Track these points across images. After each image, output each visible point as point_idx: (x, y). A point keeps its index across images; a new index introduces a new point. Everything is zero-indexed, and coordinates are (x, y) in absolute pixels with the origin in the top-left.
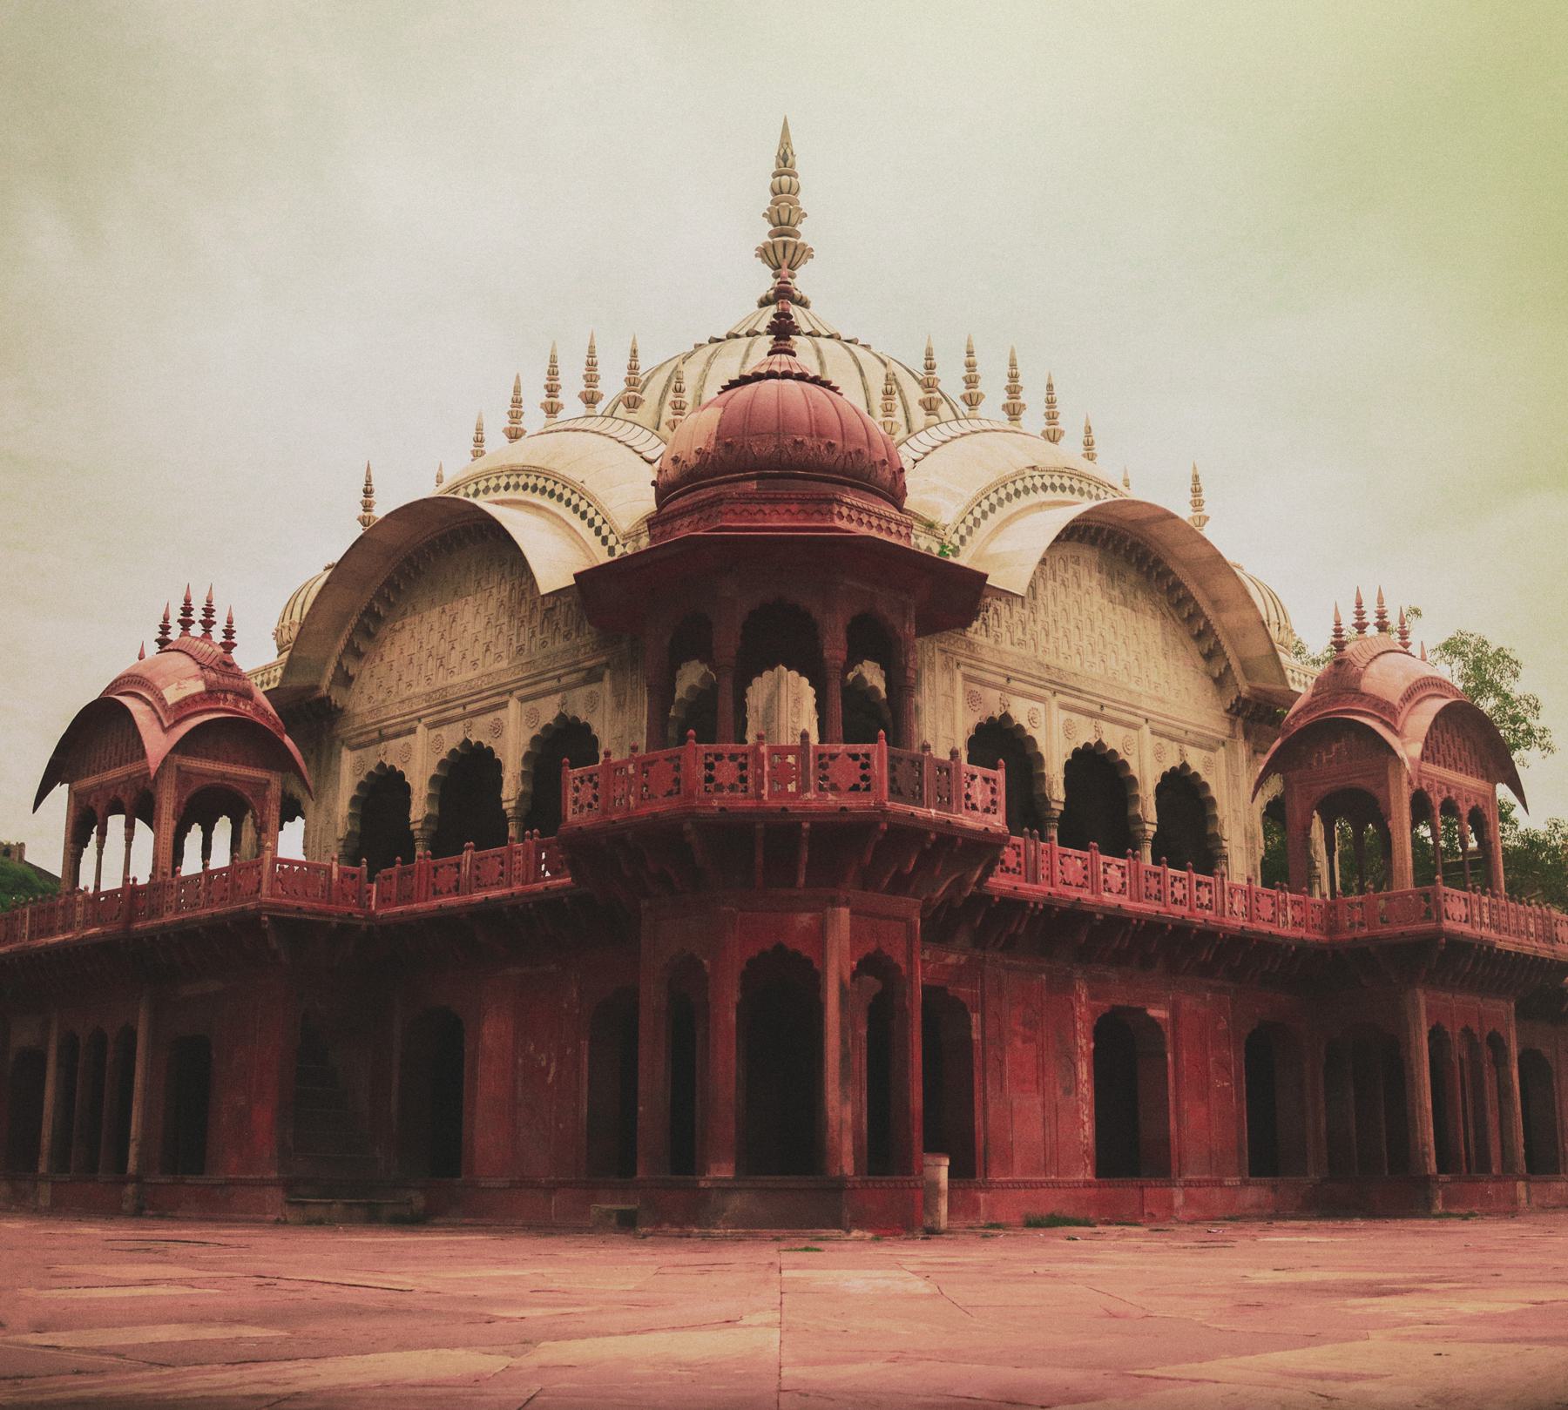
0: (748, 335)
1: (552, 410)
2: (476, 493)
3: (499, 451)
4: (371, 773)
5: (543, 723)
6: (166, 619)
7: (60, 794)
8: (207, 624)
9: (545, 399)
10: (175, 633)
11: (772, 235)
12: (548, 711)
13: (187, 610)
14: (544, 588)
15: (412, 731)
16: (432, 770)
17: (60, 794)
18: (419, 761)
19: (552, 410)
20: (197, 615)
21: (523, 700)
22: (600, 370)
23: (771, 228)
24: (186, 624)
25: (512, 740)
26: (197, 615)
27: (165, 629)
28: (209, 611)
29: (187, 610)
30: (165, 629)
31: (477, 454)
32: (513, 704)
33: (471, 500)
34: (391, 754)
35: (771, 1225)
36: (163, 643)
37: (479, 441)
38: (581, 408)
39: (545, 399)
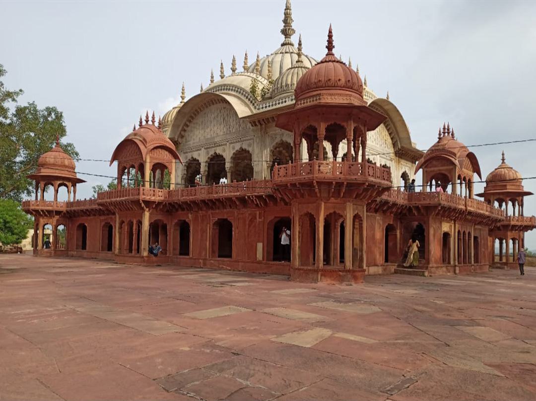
0: (281, 53)
1: (234, 70)
2: (216, 91)
3: (217, 80)
4: (189, 160)
5: (188, 158)
6: (141, 120)
7: (116, 163)
8: (153, 122)
9: (244, 65)
10: (144, 123)
11: (284, 26)
12: (237, 147)
13: (147, 117)
14: (240, 116)
15: (200, 150)
16: (231, 155)
17: (116, 163)
18: (203, 158)
19: (234, 70)
20: (150, 119)
21: (205, 148)
22: (237, 62)
23: (284, 24)
24: (147, 121)
25: (228, 154)
26: (150, 119)
27: (141, 122)
28: (153, 118)
29: (147, 117)
30: (141, 122)
31: (212, 81)
32: (203, 149)
33: (215, 93)
34: (195, 155)
35: (431, 206)
36: (141, 125)
37: (212, 77)
38: (243, 70)
39: (244, 65)
